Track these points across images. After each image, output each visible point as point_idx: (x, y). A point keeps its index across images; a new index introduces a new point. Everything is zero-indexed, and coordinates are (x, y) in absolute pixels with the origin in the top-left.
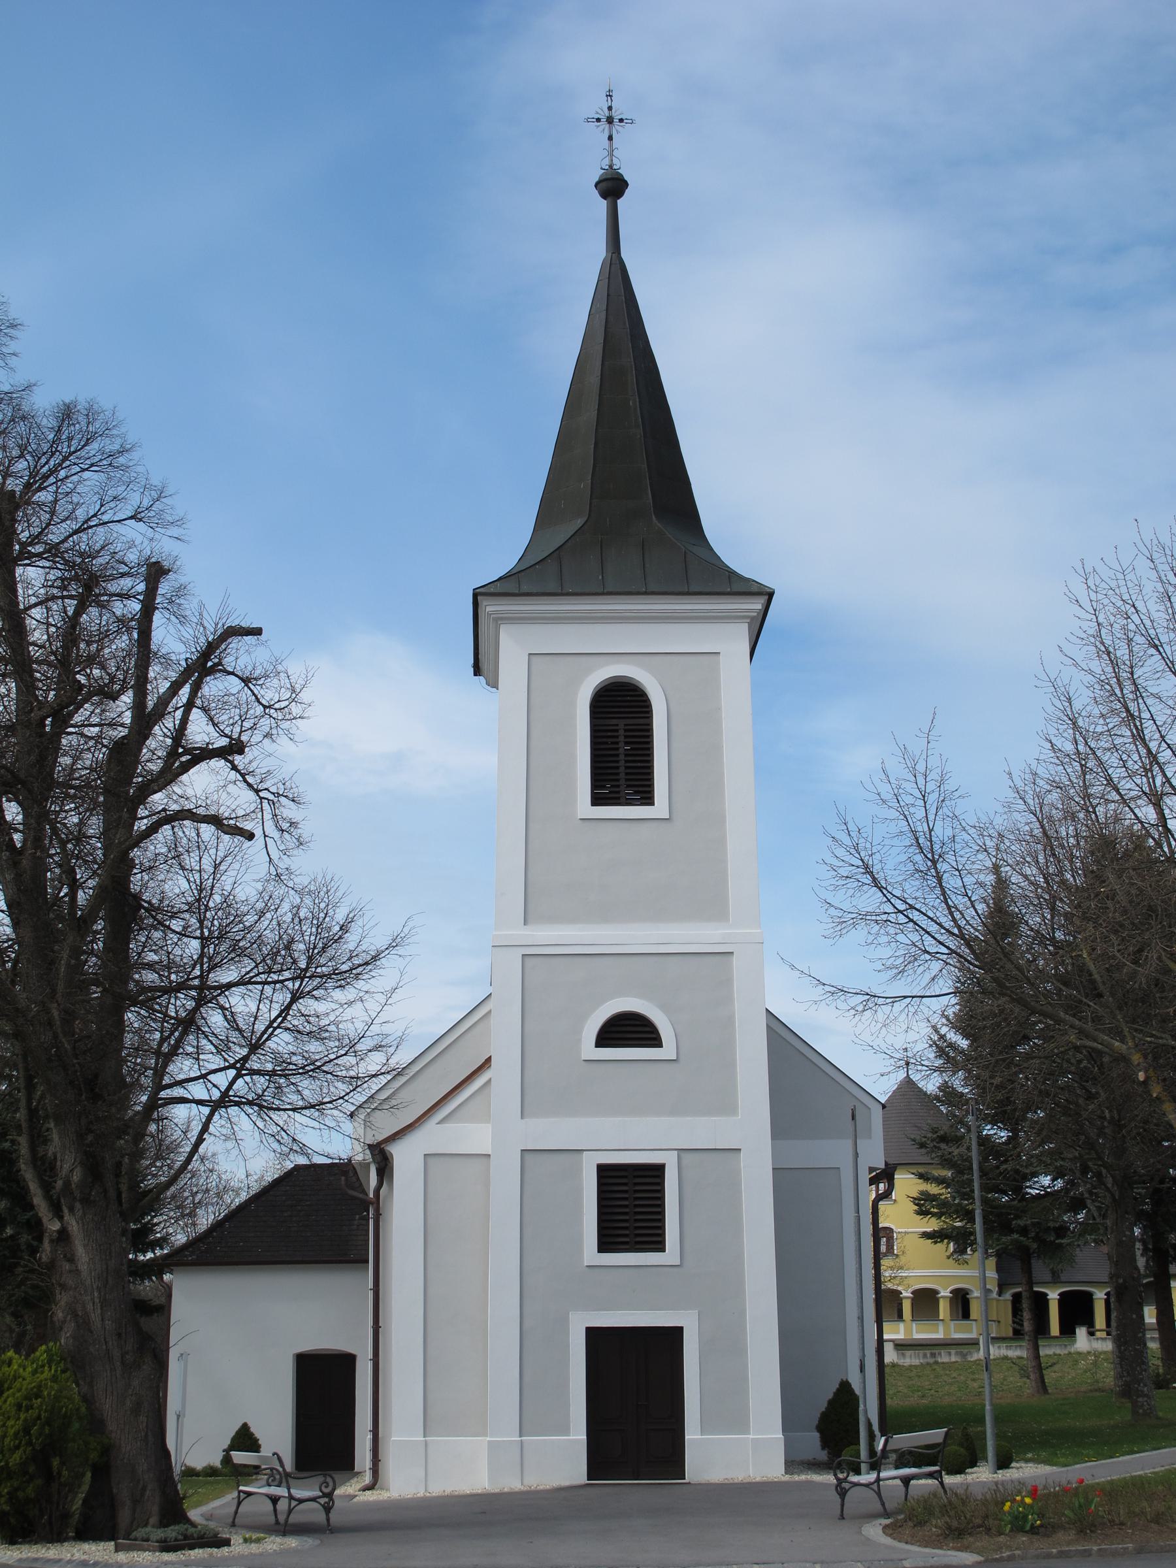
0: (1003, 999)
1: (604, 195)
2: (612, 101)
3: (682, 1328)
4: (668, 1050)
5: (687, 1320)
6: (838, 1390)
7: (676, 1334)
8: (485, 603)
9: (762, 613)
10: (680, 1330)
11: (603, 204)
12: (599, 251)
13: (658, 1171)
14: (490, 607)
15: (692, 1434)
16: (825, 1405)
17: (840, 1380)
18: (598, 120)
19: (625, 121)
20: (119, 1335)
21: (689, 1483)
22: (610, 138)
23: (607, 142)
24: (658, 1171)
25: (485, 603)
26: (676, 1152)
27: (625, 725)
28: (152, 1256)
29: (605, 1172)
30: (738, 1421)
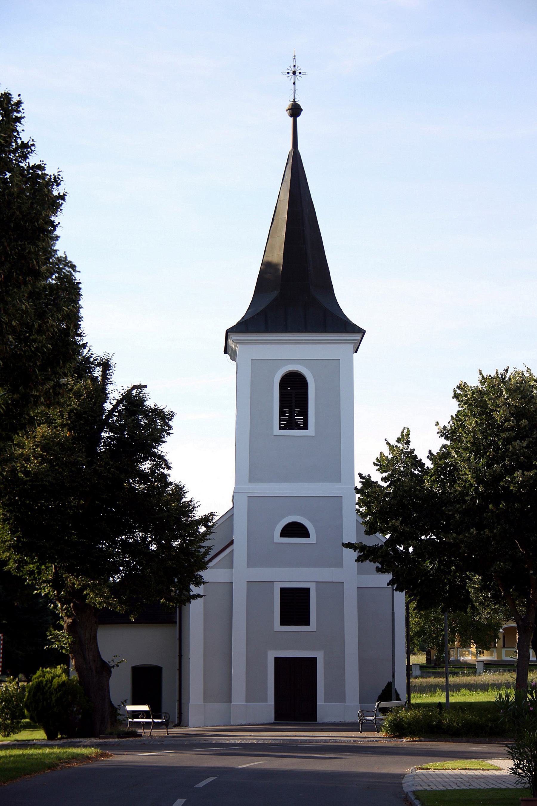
0: (52, 757)
1: (291, 115)
2: (296, 62)
3: (316, 658)
4: (313, 539)
5: (271, 656)
6: (387, 685)
7: (313, 661)
8: (231, 336)
9: (360, 341)
10: (276, 658)
11: (291, 119)
12: (289, 147)
13: (307, 590)
14: (234, 337)
15: (320, 702)
16: (381, 692)
17: (388, 681)
18: (288, 73)
19: (302, 73)
20: (95, 661)
21: (319, 723)
22: (294, 83)
23: (293, 85)
24: (307, 590)
25: (231, 336)
26: (315, 583)
27: (295, 392)
28: (443, 700)
29: (283, 591)
30: (341, 697)
